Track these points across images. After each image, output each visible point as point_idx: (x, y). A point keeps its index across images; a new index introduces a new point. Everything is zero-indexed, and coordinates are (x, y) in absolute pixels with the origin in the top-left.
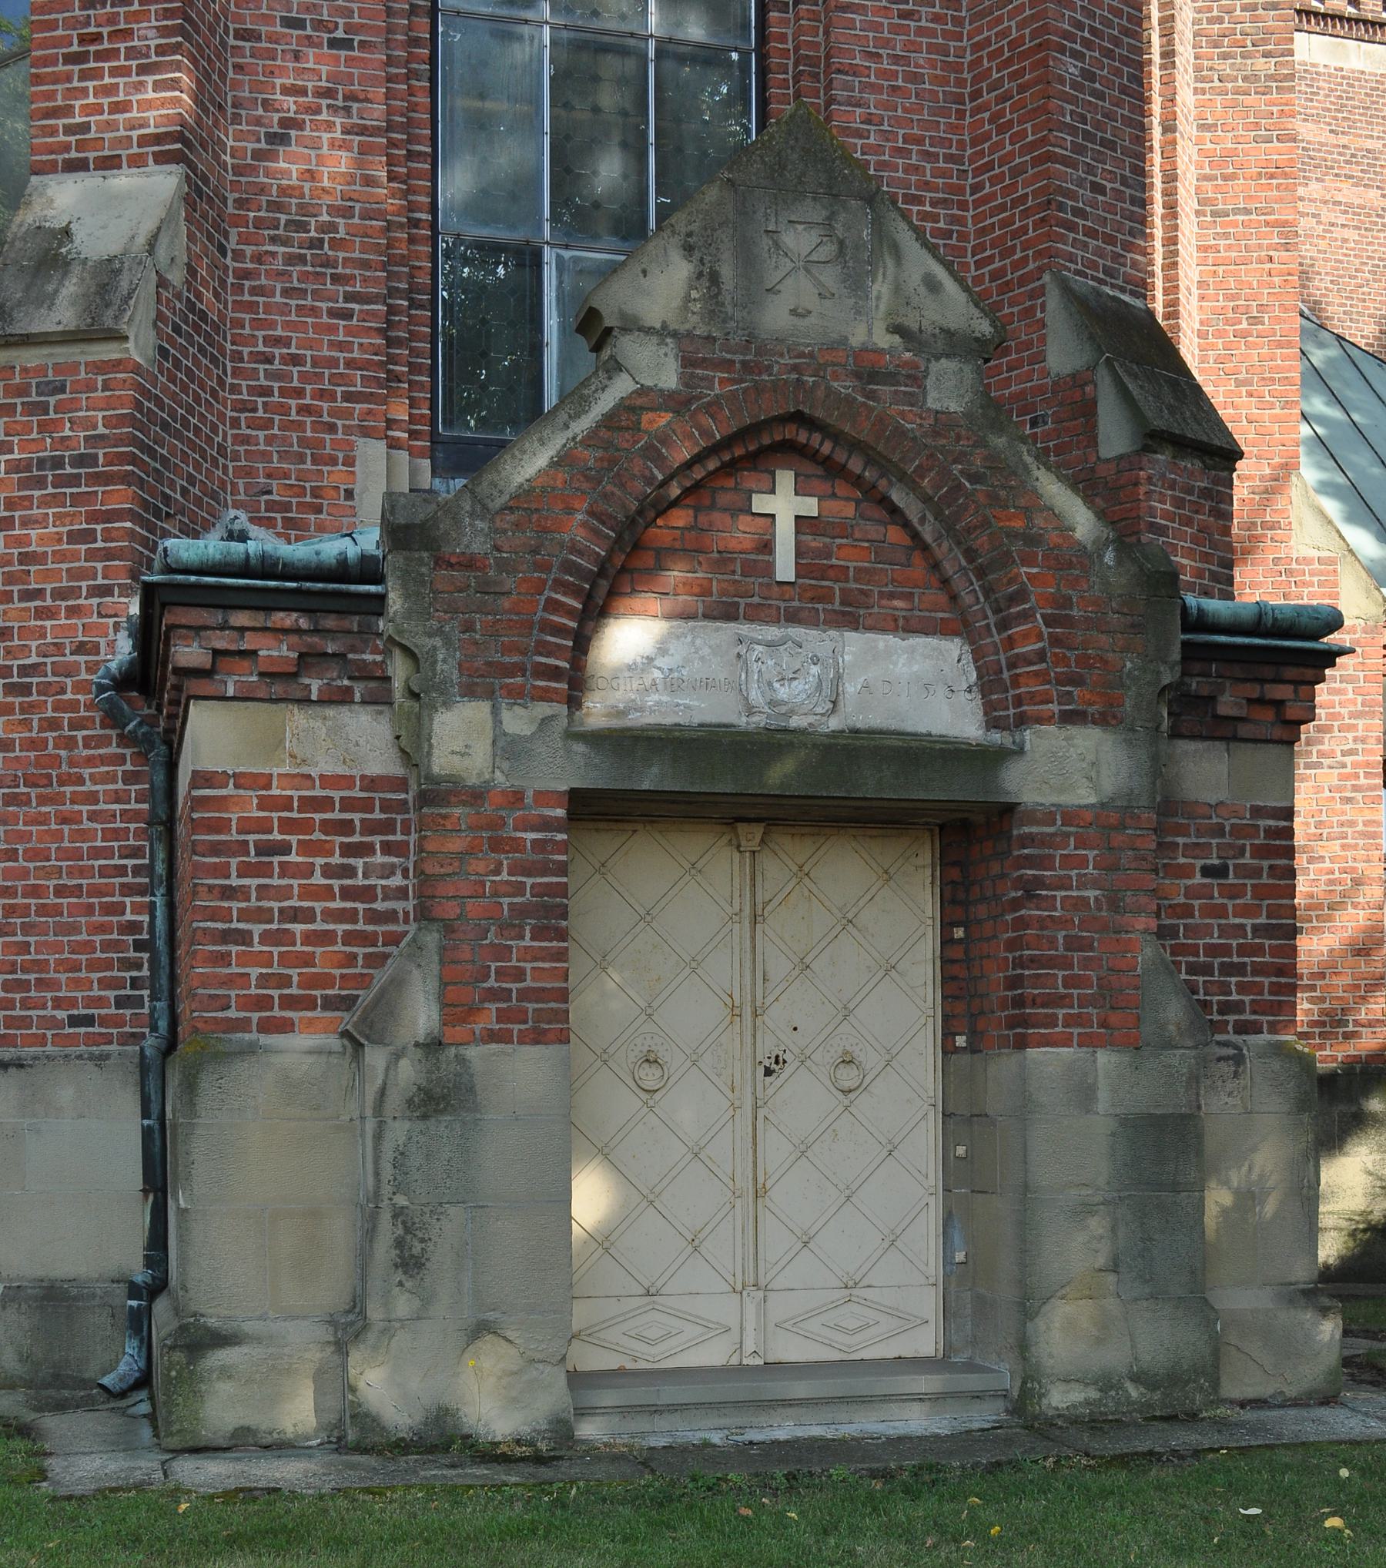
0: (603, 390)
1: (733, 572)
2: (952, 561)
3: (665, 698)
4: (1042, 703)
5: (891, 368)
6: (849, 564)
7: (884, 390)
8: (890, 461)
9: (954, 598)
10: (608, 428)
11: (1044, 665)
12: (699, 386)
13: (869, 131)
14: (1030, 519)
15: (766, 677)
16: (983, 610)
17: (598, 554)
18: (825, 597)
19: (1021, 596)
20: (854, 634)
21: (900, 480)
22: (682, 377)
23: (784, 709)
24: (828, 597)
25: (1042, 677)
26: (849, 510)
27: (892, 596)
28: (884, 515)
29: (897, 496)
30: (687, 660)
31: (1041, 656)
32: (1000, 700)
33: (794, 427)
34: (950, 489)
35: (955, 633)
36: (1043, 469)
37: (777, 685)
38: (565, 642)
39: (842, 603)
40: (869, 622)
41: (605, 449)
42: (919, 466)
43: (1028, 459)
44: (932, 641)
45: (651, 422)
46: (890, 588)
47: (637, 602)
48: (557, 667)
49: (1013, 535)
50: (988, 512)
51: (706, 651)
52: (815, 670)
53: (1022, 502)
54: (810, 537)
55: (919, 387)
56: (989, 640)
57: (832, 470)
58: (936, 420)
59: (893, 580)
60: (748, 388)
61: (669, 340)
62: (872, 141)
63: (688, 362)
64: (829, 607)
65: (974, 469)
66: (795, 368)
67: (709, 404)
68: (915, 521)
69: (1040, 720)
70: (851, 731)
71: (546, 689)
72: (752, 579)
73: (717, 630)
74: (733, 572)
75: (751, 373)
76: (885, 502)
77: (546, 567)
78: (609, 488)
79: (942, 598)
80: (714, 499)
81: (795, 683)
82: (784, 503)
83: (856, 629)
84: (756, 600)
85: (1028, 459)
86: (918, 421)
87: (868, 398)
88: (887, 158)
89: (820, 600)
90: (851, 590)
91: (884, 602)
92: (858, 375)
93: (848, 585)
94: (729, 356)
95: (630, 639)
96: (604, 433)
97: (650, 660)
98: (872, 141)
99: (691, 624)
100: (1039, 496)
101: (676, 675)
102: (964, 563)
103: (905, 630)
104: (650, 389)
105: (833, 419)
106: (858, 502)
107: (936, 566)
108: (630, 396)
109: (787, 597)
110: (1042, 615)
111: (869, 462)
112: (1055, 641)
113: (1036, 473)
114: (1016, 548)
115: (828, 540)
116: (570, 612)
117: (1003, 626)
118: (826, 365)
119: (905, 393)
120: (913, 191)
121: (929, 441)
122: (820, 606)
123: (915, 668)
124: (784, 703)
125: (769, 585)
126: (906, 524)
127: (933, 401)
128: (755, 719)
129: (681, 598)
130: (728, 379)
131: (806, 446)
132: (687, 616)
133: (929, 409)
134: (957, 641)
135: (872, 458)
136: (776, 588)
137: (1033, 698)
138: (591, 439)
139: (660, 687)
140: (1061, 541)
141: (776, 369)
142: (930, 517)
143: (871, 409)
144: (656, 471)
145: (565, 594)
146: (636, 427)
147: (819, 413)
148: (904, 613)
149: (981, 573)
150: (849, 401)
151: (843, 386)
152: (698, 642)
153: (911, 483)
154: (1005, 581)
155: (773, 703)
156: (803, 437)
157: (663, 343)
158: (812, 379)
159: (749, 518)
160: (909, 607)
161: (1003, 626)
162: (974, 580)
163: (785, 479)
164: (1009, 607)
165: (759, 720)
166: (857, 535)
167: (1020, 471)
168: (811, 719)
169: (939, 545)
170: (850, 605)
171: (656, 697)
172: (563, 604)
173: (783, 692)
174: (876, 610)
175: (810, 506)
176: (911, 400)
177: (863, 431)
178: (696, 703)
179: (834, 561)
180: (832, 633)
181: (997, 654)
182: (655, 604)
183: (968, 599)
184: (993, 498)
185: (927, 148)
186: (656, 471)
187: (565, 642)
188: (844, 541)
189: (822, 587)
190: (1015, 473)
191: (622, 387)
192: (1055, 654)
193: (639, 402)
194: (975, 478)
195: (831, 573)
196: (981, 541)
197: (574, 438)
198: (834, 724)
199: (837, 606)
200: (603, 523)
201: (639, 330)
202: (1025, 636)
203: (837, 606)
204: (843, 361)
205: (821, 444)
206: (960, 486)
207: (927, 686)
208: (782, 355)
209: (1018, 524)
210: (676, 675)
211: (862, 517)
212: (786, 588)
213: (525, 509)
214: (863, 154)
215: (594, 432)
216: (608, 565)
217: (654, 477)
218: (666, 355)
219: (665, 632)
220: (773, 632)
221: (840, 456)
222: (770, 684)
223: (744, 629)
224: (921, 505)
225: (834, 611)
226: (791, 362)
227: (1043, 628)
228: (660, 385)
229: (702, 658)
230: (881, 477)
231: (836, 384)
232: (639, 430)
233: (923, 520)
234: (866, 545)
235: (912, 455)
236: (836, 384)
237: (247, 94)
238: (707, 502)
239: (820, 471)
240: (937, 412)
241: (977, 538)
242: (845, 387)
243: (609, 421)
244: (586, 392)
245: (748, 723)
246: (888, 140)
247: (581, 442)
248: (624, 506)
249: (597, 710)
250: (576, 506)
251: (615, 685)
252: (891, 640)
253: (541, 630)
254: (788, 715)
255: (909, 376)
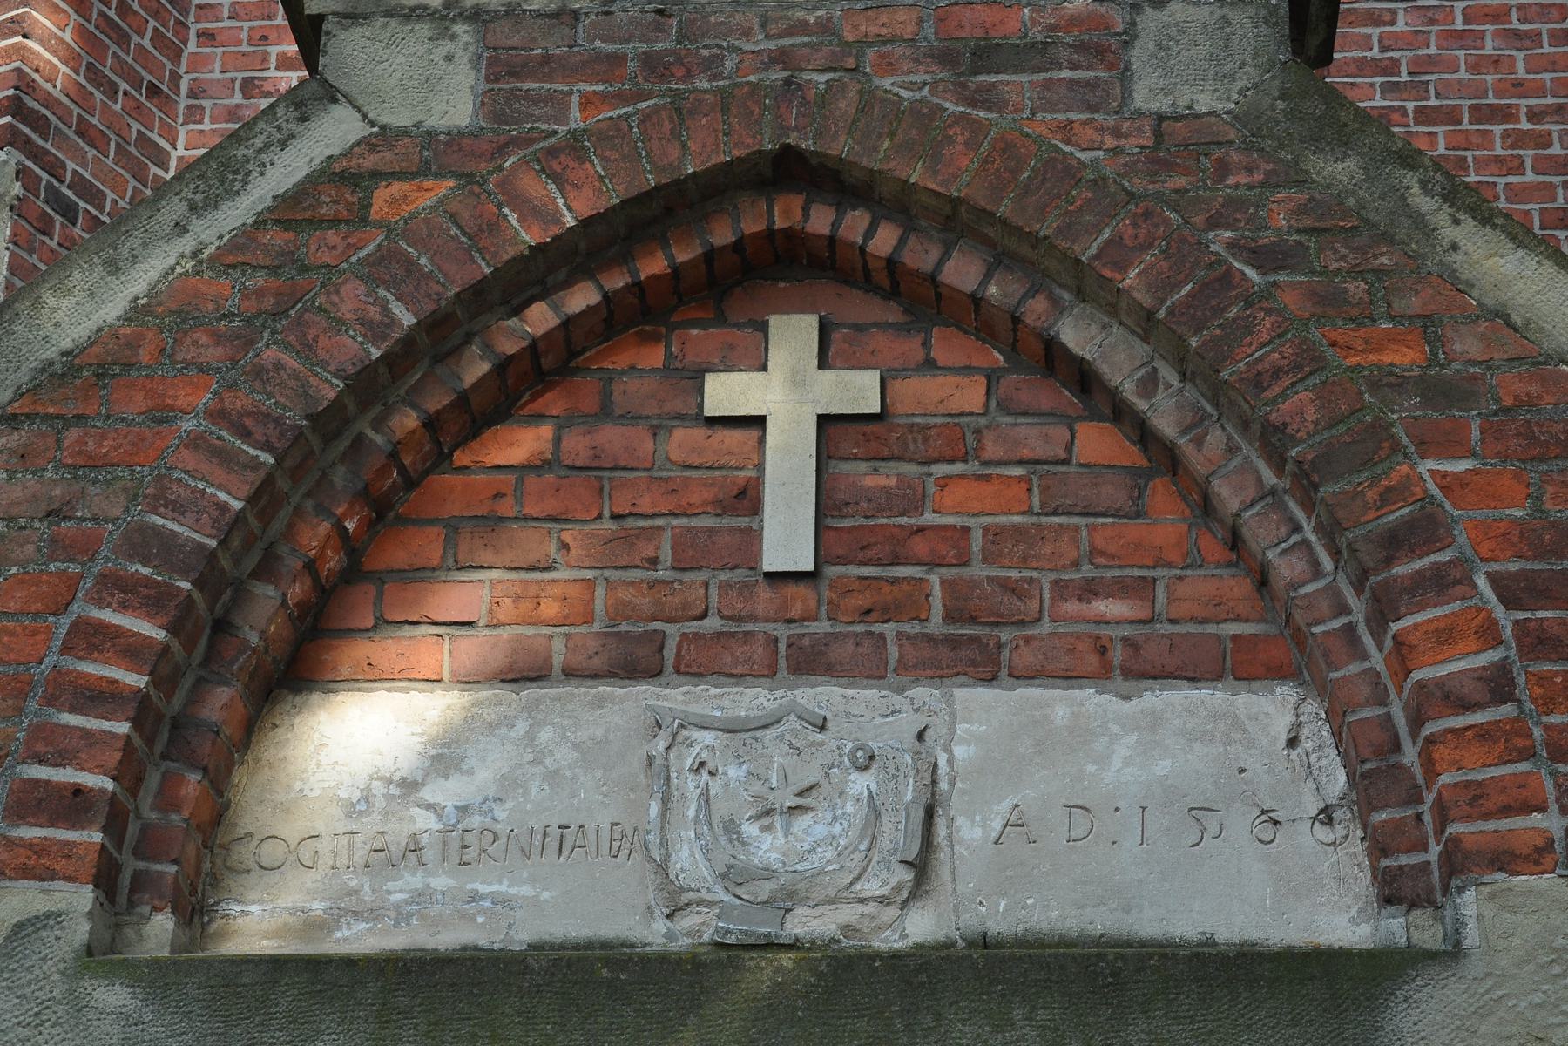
0: (283, 144)
1: (654, 562)
2: (1237, 477)
3: (441, 882)
4: (1506, 811)
5: (1036, 34)
6: (970, 522)
7: (1017, 84)
8: (1036, 241)
9: (1263, 580)
10: (285, 224)
11: (1507, 710)
12: (529, 117)
13: (1394, 12)
14: (1435, 341)
15: (720, 809)
16: (1332, 591)
17: (223, 508)
18: (907, 605)
19: (1425, 530)
20: (983, 693)
21: (1081, 295)
22: (485, 101)
23: (765, 890)
24: (897, 599)
25: (1507, 741)
26: (970, 395)
27: (1089, 590)
28: (1068, 398)
29: (1076, 335)
30: (509, 784)
31: (1498, 685)
32: (1398, 825)
33: (797, 202)
34: (1203, 287)
35: (1279, 672)
36: (1469, 223)
37: (750, 830)
38: (106, 725)
39: (949, 617)
40: (1027, 658)
41: (274, 270)
42: (1115, 242)
43: (1422, 202)
44: (1211, 697)
45: (394, 202)
46: (1087, 570)
47: (386, 649)
48: (78, 790)
49: (1389, 383)
50: (1315, 333)
51: (564, 756)
52: (860, 783)
53: (1413, 304)
54: (863, 466)
55: (1111, 67)
56: (1354, 668)
57: (921, 301)
58: (1158, 135)
59: (1094, 552)
60: (656, 110)
61: (459, 28)
62: (1401, 26)
63: (501, 68)
64: (914, 628)
65: (1267, 238)
66: (781, 58)
67: (552, 152)
68: (1129, 391)
69: (1505, 859)
70: (971, 944)
71: (40, 849)
72: (702, 576)
73: (600, 703)
74: (654, 562)
75: (662, 78)
76: (1054, 360)
77: (85, 549)
78: (271, 354)
79: (1238, 587)
80: (606, 395)
81: (802, 822)
82: (781, 387)
83: (991, 679)
84: (712, 623)
85: (1422, 202)
86: (1110, 142)
87: (973, 103)
88: (1433, 50)
89: (888, 613)
90: (973, 584)
91: (1072, 607)
92: (945, 57)
93: (966, 572)
94: (609, 48)
95: (359, 740)
96: (275, 238)
97: (409, 786)
98: (1401, 26)
99: (530, 692)
100: (1460, 287)
101: (476, 821)
102: (1269, 478)
103: (1128, 674)
104: (404, 132)
105: (882, 157)
106: (992, 378)
107: (1206, 506)
108: (348, 154)
109: (796, 612)
110: (1494, 579)
111: (1000, 260)
112: (1535, 642)
113: (1449, 233)
114: (1401, 415)
115: (912, 469)
116: (131, 650)
117: (1381, 616)
118: (863, 43)
119: (1072, 83)
120: (1491, 100)
121: (1138, 184)
122: (889, 629)
123: (1163, 767)
124: (769, 873)
125: (746, 587)
126: (1120, 413)
127: (1148, 93)
128: (688, 921)
129: (506, 633)
130: (604, 97)
131: (832, 240)
132: (523, 673)
133: (1139, 114)
134: (1286, 692)
135: (1008, 248)
136: (765, 593)
137: (1476, 799)
138: (232, 256)
139: (429, 855)
140: (1535, 389)
141: (730, 64)
142: (1168, 374)
143: (978, 130)
144: (398, 309)
145: (123, 607)
146: (361, 217)
147: (841, 146)
148: (1127, 631)
149: (1306, 483)
150: (925, 116)
151: (903, 85)
152: (545, 736)
153: (1090, 287)
154: (1371, 495)
155: (732, 876)
156: (820, 221)
157: (446, 34)
158: (823, 78)
159: (700, 433)
160: (1141, 612)
161: (1381, 616)
162: (1300, 515)
163: (792, 335)
164: (1389, 562)
165: (695, 929)
166: (992, 450)
167: (1401, 233)
168: (848, 914)
169: (1199, 442)
170: (973, 620)
171: (415, 880)
172: (115, 633)
173: (767, 847)
174: (1046, 627)
175: (858, 390)
176: (1090, 97)
177: (958, 174)
178: (527, 890)
179: (929, 518)
180: (923, 693)
181: (1383, 701)
182: (443, 654)
183: (1286, 568)
184: (1328, 301)
185: (1515, 24)
186: (398, 309)
187: (106, 725)
188: (959, 468)
189: (894, 581)
190: (1387, 238)
191: (334, 132)
192: (1541, 679)
193: (369, 162)
194: (1265, 258)
195: (920, 546)
196: (1299, 406)
197: (195, 254)
198: (921, 926)
199: (936, 624)
200: (245, 434)
201: (389, 14)
202: (1445, 636)
203: (936, 624)
204: (908, 32)
205: (870, 233)
206: (1227, 278)
207: (1198, 812)
208: (747, 34)
209: (1404, 358)
210: (476, 821)
211: (1006, 408)
212: (792, 589)
213: (47, 417)
214: (1383, 50)
215: (246, 237)
216: (283, 550)
217: (392, 322)
218: (449, 58)
219: (458, 718)
220: (753, 699)
221: (921, 256)
222: (731, 828)
223: (674, 697)
224: (1142, 350)
225: (929, 639)
226: (772, 45)
227: (1499, 612)
228: (432, 122)
229: (553, 777)
230: (1033, 292)
231: (887, 83)
232: (364, 221)
233: (1149, 385)
234: (1018, 471)
235: (1090, 218)
236: (887, 83)
237: (217, 75)
238: (590, 403)
239: (893, 313)
240: (1161, 118)
241: (1283, 395)
242: (909, 86)
243: (292, 211)
244: (241, 152)
245: (670, 935)
246: (1432, 22)
247: (211, 258)
248: (304, 393)
249: (257, 923)
250: (182, 402)
251: (306, 857)
252: (1091, 701)
253: (50, 701)
254: (786, 901)
255: (1081, 47)
